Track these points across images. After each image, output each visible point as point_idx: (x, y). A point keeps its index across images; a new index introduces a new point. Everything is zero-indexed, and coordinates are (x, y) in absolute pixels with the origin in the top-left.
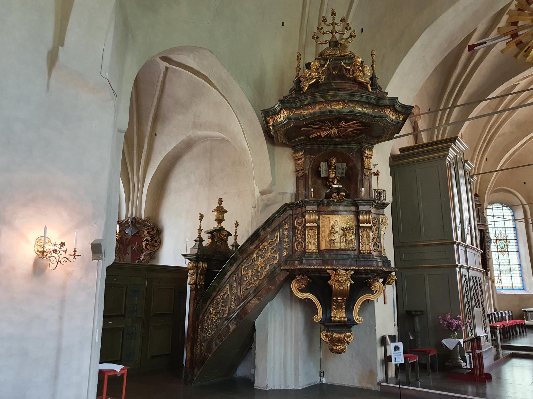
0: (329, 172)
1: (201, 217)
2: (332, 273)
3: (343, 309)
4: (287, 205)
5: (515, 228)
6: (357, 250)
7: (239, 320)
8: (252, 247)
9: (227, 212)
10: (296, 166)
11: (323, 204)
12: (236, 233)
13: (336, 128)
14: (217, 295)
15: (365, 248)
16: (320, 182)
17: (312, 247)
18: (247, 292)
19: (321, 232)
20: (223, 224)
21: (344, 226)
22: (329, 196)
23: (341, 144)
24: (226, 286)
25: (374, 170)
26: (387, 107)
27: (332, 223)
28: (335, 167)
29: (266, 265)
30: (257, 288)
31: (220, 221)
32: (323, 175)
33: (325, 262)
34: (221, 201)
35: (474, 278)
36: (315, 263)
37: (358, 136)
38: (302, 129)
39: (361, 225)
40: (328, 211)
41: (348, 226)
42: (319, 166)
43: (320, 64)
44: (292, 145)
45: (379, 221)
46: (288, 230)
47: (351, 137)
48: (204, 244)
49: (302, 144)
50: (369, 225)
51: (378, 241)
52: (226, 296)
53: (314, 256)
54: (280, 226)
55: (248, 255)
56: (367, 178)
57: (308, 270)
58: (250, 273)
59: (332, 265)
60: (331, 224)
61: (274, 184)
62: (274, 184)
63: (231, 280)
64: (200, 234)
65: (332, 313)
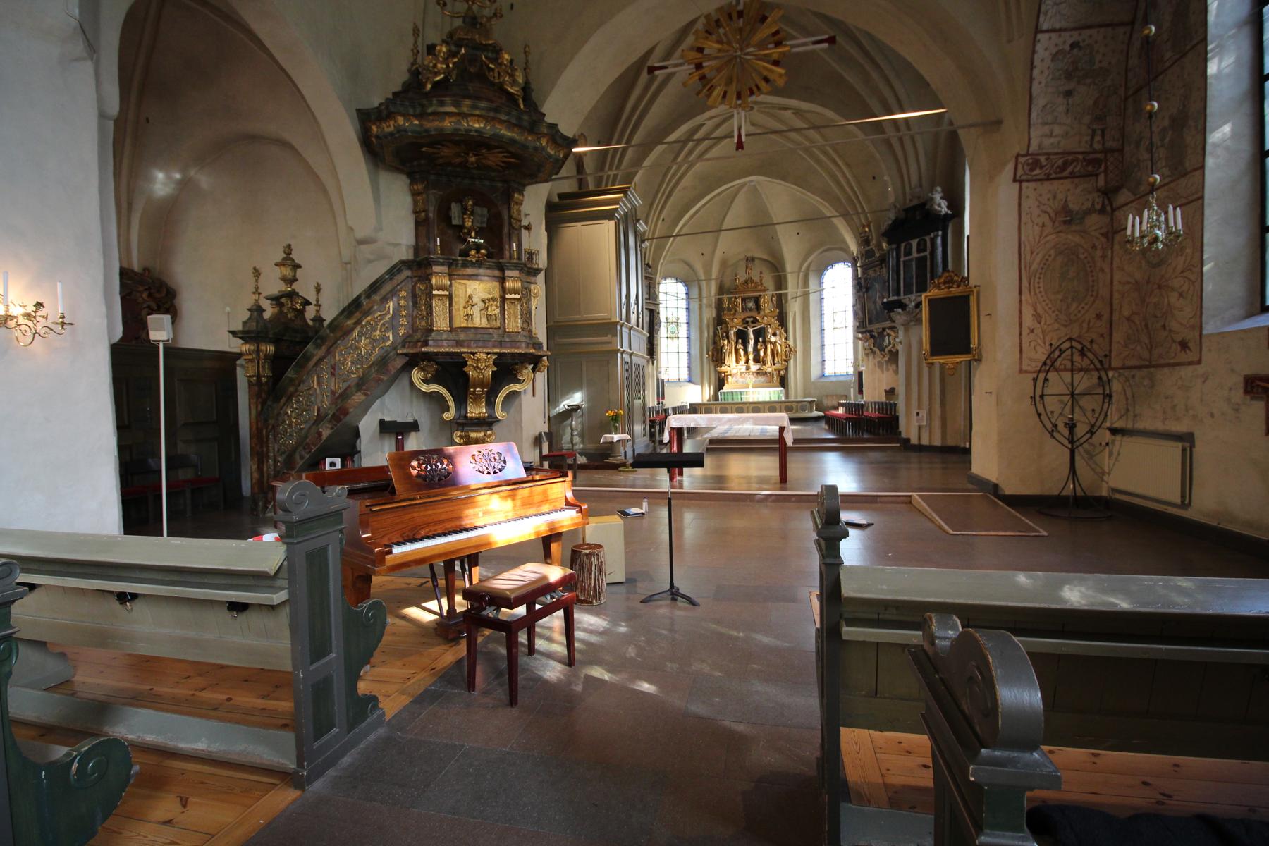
1: (257, 273)
4: (403, 262)
5: (688, 309)
8: (350, 322)
12: (317, 301)
16: (450, 232)
18: (346, 385)
21: (486, 296)
22: (465, 254)
25: (525, 222)
26: (545, 135)
29: (374, 348)
32: (455, 222)
33: (459, 343)
34: (288, 249)
35: (637, 365)
42: (449, 208)
43: (449, 51)
46: (405, 299)
48: (267, 315)
50: (517, 296)
51: (527, 318)
54: (393, 293)
59: (469, 347)
61: (381, 229)
62: (381, 229)
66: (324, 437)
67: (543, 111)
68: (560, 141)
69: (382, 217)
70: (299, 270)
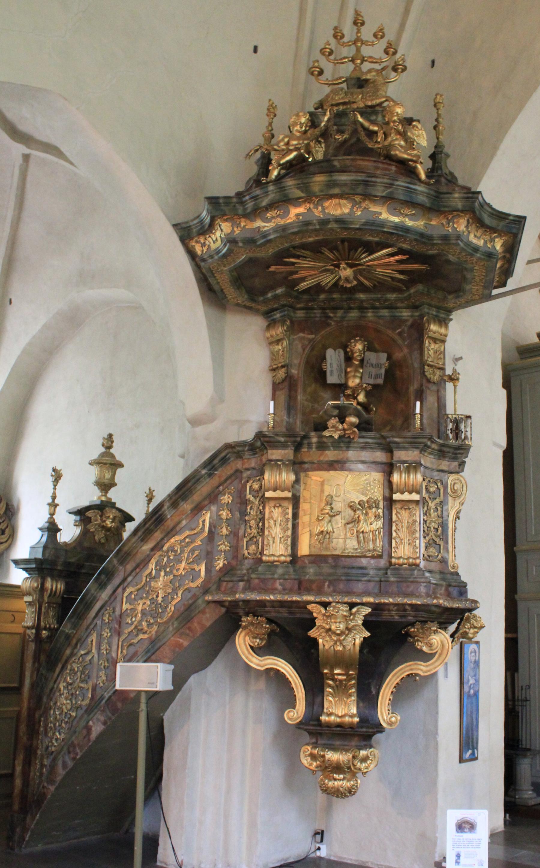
0: (346, 373)
1: (57, 476)
2: (316, 610)
3: (350, 695)
6: (385, 557)
7: (110, 714)
8: (147, 547)
9: (121, 465)
10: (272, 359)
11: (310, 445)
13: (351, 266)
14: (72, 654)
15: (402, 552)
17: (277, 549)
19: (301, 513)
20: (113, 495)
21: (356, 497)
23: (374, 308)
24: (89, 634)
27: (328, 490)
28: (362, 361)
29: (175, 591)
30: (153, 642)
31: (105, 486)
32: (332, 379)
33: (302, 586)
34: (109, 442)
36: (280, 587)
37: (408, 288)
38: (272, 269)
39: (396, 497)
40: (319, 462)
41: (365, 499)
44: (264, 308)
45: (446, 488)
47: (394, 290)
49: (284, 306)
50: (415, 497)
52: (89, 658)
53: (280, 571)
54: (213, 497)
55: (137, 566)
56: (434, 388)
57: (262, 604)
58: (140, 608)
60: (326, 494)
63: (99, 622)
64: (52, 514)
65: (326, 705)
66: (94, 735)
67: (498, 190)
68: (487, 220)
69: (224, 378)
70: (119, 471)
